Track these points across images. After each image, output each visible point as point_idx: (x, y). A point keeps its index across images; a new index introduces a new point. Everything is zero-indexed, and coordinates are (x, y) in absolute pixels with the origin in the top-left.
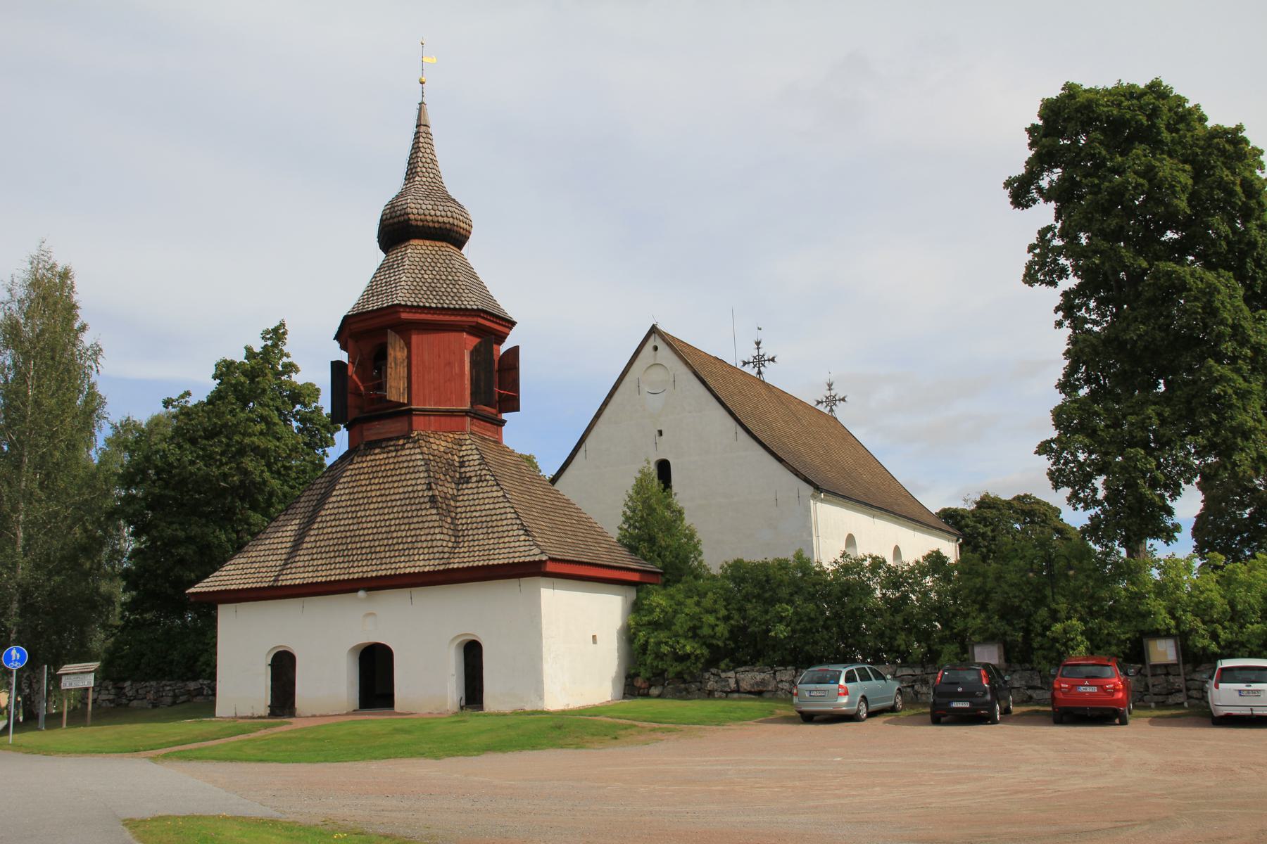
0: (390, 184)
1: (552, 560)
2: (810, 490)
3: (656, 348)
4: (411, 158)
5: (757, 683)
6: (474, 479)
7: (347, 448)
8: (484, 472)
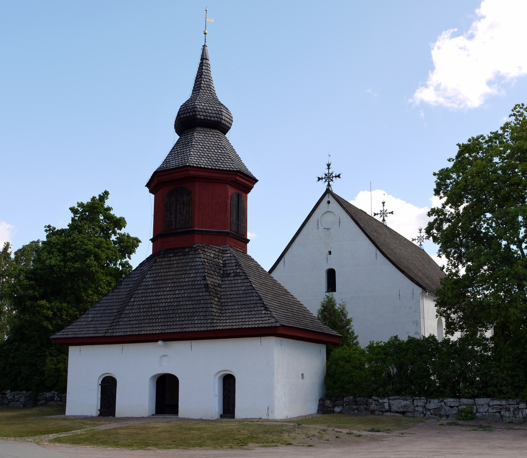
0: (185, 94)
1: (282, 326)
2: (420, 290)
3: (329, 202)
4: (197, 78)
5: (402, 407)
6: (232, 275)
7: (151, 253)
8: (238, 271)
